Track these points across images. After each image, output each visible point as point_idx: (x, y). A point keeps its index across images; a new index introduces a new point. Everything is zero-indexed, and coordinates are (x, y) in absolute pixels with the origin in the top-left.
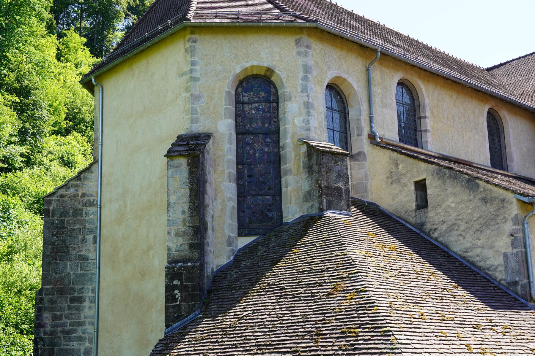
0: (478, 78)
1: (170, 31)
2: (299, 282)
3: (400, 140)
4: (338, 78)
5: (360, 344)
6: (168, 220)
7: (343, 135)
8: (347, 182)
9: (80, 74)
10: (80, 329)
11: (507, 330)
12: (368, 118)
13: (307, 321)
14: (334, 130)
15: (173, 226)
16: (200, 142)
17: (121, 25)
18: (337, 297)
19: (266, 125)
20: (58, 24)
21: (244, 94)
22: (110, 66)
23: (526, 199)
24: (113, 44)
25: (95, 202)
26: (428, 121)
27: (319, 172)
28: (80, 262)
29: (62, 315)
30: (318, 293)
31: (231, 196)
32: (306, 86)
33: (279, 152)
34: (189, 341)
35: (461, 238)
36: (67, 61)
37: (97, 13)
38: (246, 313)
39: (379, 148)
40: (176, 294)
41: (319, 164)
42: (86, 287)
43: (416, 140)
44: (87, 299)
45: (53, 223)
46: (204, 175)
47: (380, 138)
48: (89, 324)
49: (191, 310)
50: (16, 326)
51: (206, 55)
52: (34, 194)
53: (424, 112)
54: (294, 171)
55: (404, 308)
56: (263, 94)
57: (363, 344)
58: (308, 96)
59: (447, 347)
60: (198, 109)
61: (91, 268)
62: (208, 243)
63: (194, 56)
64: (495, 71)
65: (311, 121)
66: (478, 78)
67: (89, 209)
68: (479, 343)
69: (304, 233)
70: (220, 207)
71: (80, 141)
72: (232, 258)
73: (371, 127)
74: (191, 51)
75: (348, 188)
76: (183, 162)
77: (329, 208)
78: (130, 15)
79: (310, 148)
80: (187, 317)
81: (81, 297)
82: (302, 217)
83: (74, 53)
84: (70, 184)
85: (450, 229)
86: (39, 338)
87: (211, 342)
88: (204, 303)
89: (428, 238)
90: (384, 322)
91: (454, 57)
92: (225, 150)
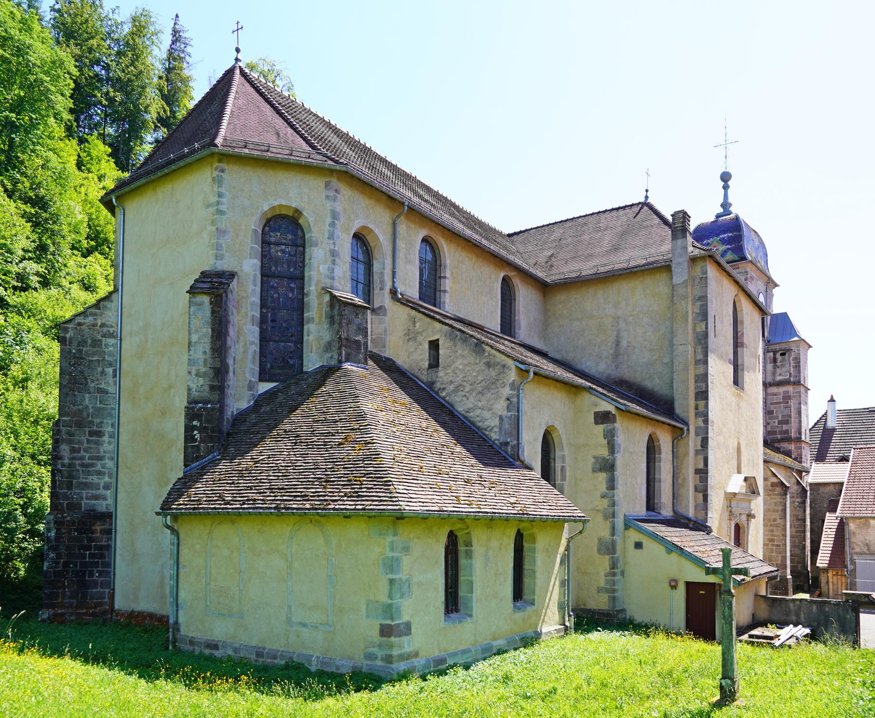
0: (498, 243)
1: (197, 156)
2: (314, 431)
3: (421, 298)
4: (364, 228)
5: (363, 492)
6: (189, 359)
7: (367, 287)
8: (366, 336)
9: (104, 188)
10: (99, 463)
11: (493, 486)
12: (391, 273)
13: (318, 468)
14: (357, 282)
15: (194, 365)
16: (224, 281)
17: (149, 138)
18: (347, 447)
19: (292, 270)
20: (78, 126)
21: (271, 233)
22: (132, 186)
23: (523, 367)
24: (141, 158)
25: (115, 334)
26: (447, 281)
27: (340, 323)
28: (99, 395)
29: (80, 448)
30: (330, 442)
31: (253, 339)
32: (333, 233)
33: (303, 299)
34: (206, 481)
35: (465, 399)
36: (89, 171)
37: (124, 120)
38: (262, 457)
39: (399, 304)
40: (195, 435)
41: (340, 315)
42: (105, 421)
43: (435, 299)
44: (107, 434)
45: (70, 352)
46: (227, 316)
47: (401, 294)
48: (109, 459)
49: (209, 451)
50: (33, 457)
51: (234, 188)
52: (51, 318)
53: (445, 272)
54: (317, 320)
55: (406, 460)
56: (290, 236)
57: (366, 492)
58: (334, 243)
59: (439, 498)
60: (223, 246)
61: (111, 402)
62: (229, 386)
63: (221, 187)
64: (515, 238)
65: (335, 270)
66: (498, 243)
67: (108, 340)
68: (467, 495)
69: (322, 383)
70: (242, 350)
71: (103, 264)
72: (252, 402)
73: (394, 282)
74: (219, 181)
75: (367, 342)
76: (206, 299)
77: (347, 360)
78: (159, 127)
79: (333, 297)
80: (205, 457)
81: (100, 431)
82: (321, 367)
83: (97, 163)
84: (88, 313)
85: (456, 390)
86: (57, 470)
87: (227, 483)
88: (223, 445)
89: (437, 397)
90: (386, 472)
91: (479, 219)
92: (250, 291)
